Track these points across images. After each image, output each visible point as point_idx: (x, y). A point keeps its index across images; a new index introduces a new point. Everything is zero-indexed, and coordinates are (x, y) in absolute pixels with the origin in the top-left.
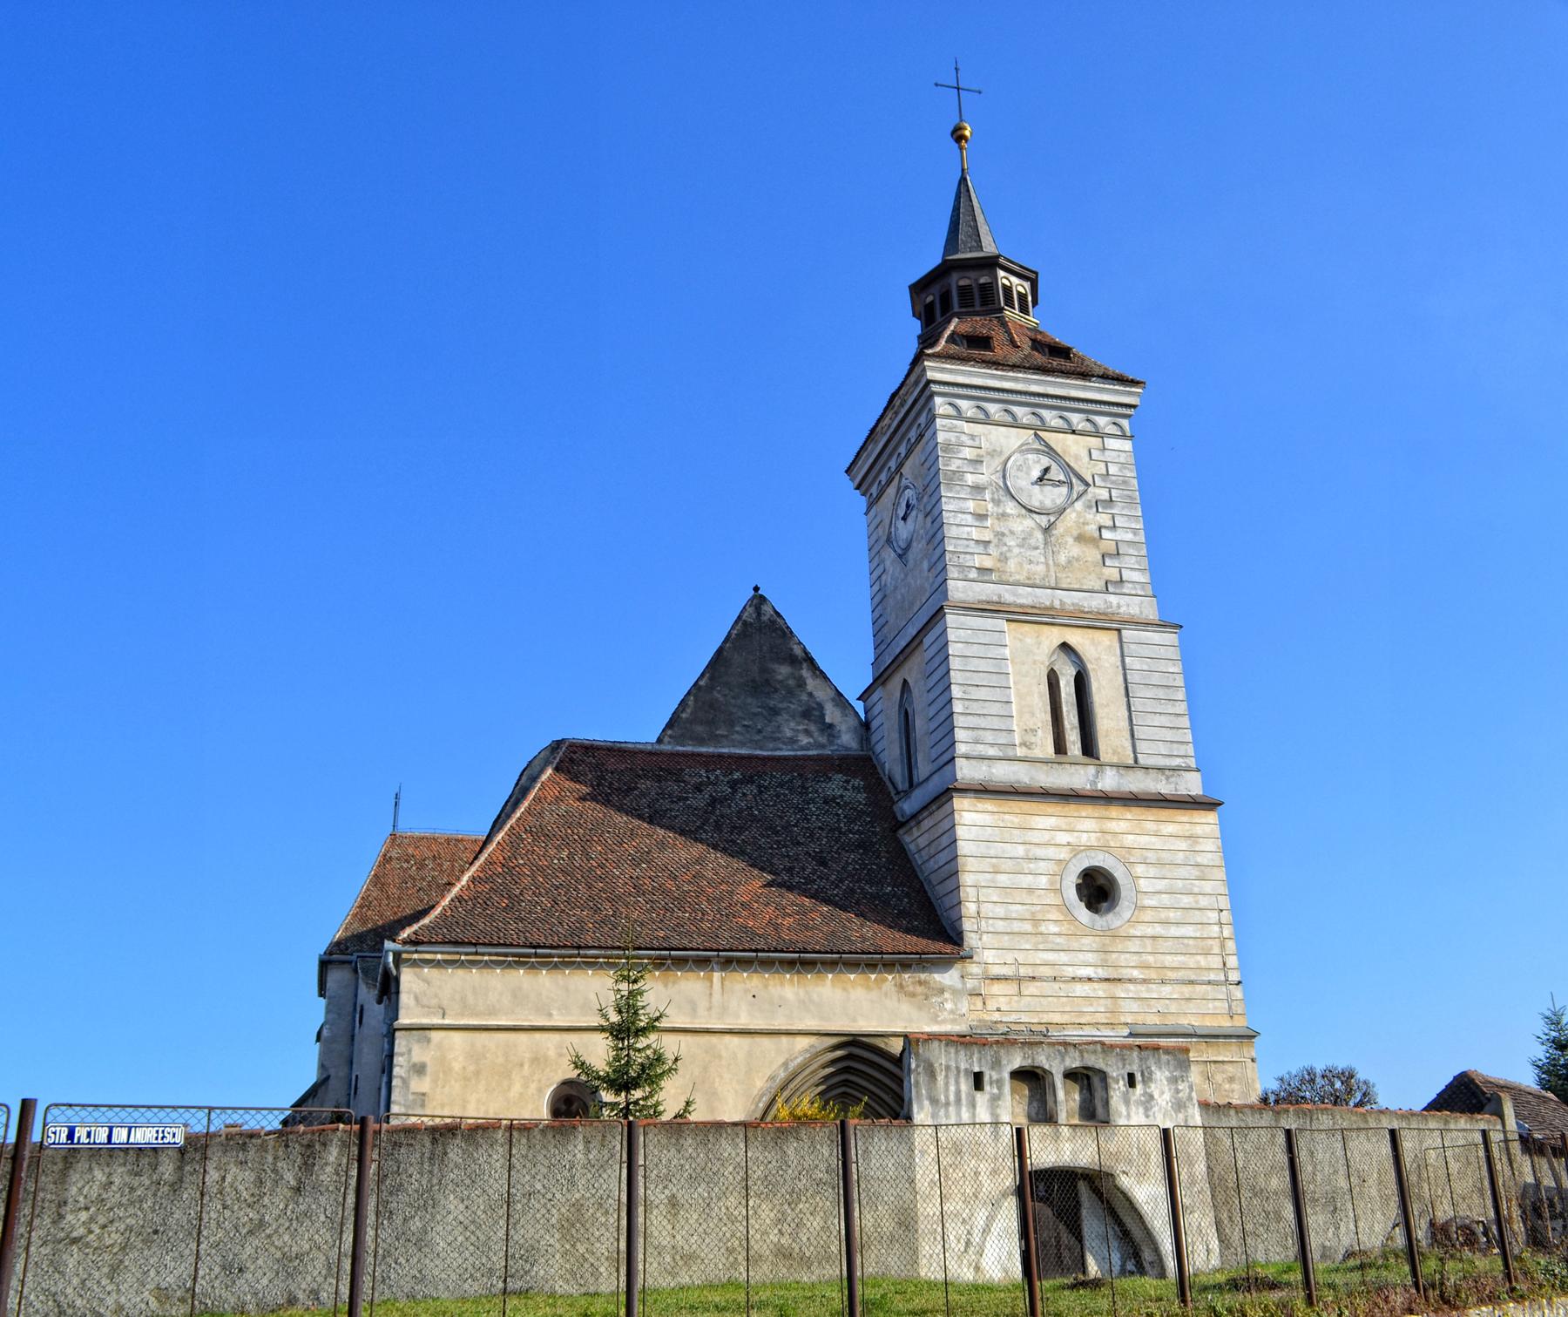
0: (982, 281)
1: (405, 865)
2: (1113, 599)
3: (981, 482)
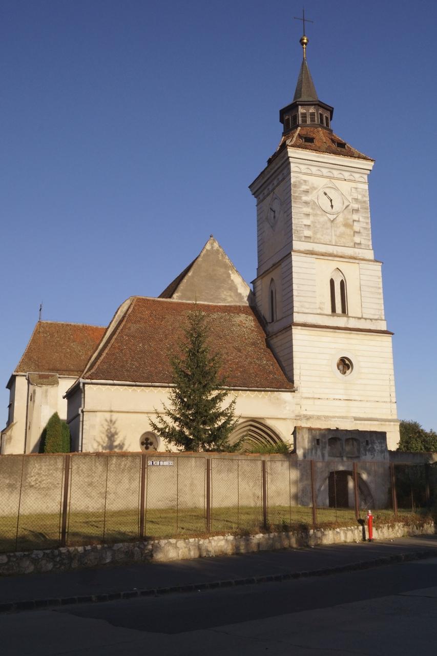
0: (311, 111)
1: (45, 335)
2: (356, 250)
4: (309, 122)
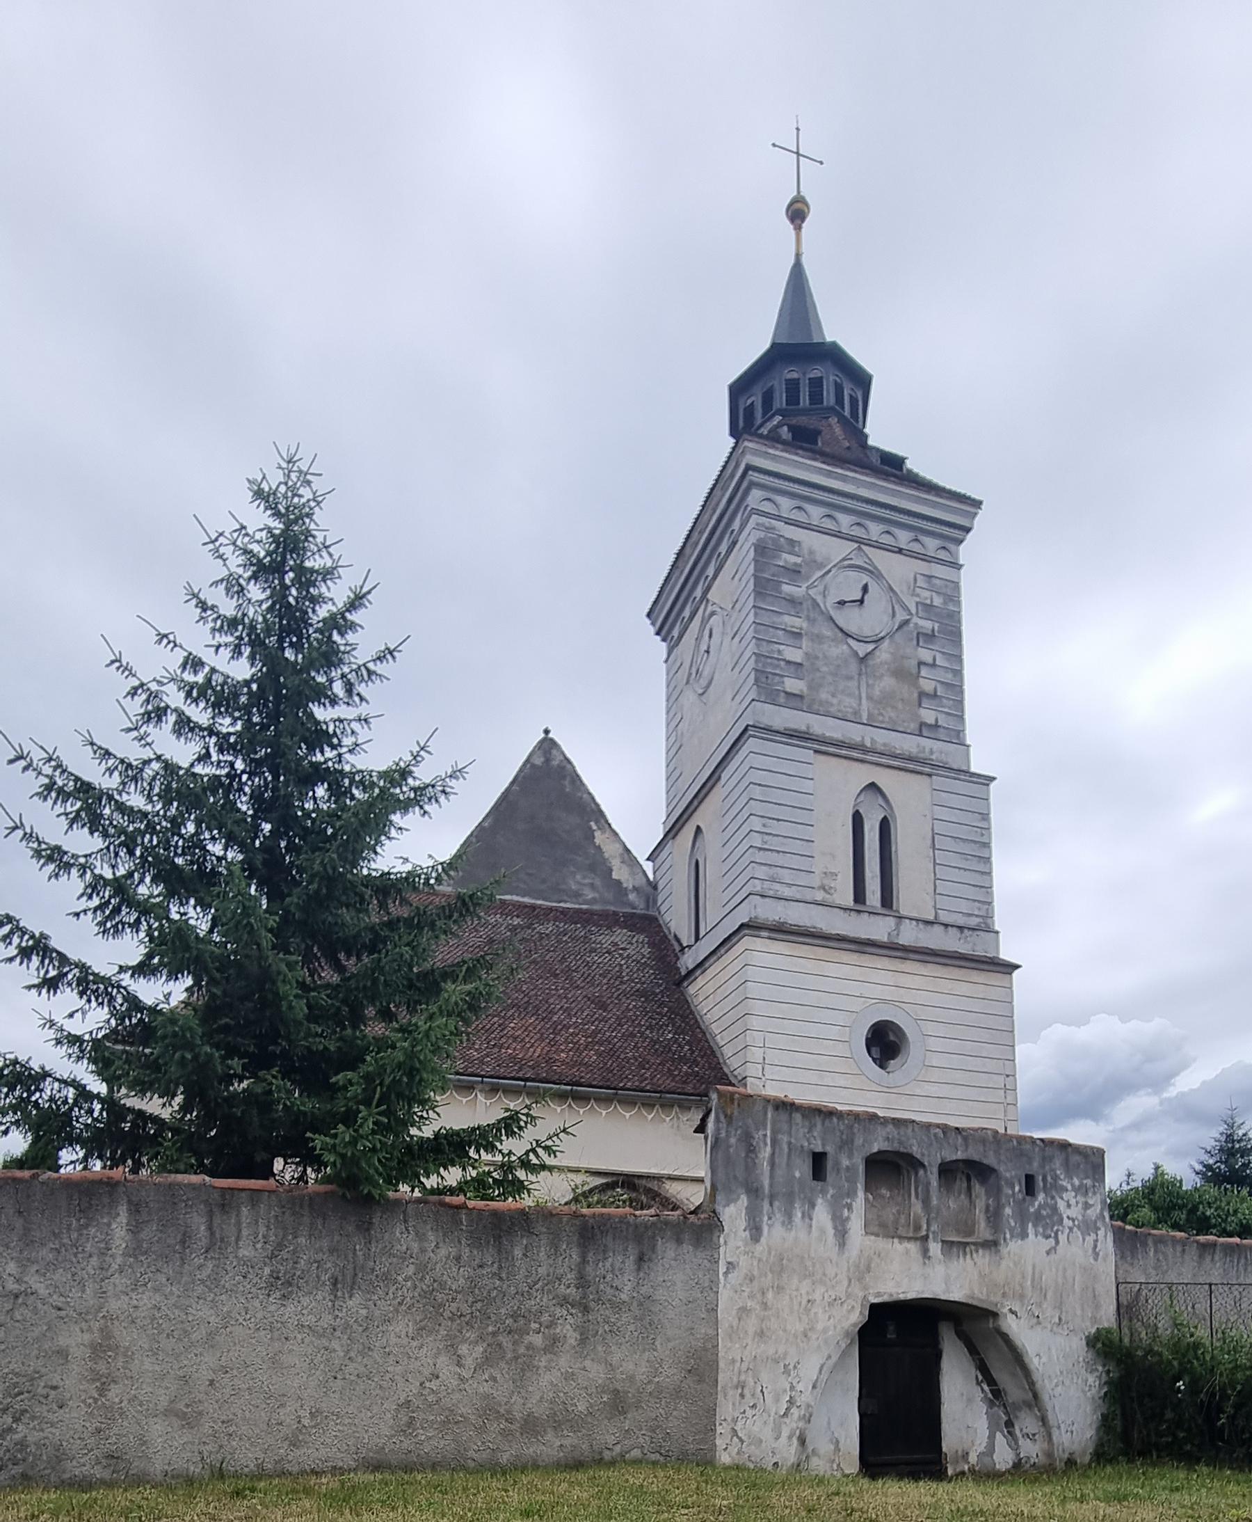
2: (927, 743)
3: (796, 595)
4: (805, 401)
